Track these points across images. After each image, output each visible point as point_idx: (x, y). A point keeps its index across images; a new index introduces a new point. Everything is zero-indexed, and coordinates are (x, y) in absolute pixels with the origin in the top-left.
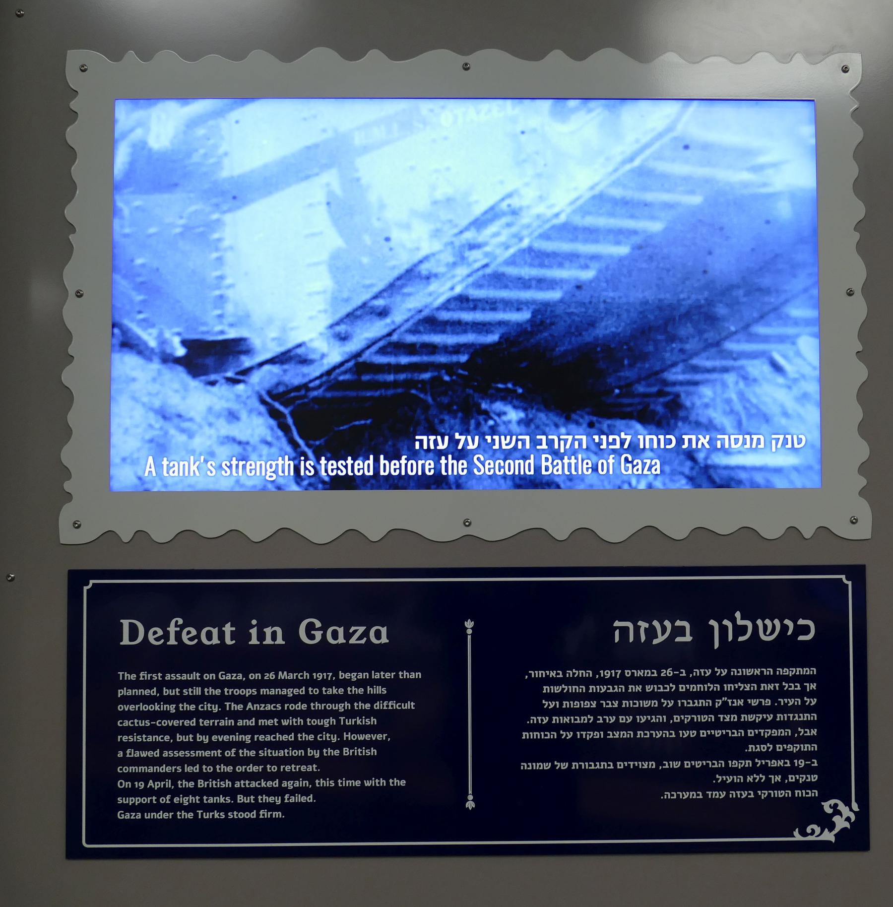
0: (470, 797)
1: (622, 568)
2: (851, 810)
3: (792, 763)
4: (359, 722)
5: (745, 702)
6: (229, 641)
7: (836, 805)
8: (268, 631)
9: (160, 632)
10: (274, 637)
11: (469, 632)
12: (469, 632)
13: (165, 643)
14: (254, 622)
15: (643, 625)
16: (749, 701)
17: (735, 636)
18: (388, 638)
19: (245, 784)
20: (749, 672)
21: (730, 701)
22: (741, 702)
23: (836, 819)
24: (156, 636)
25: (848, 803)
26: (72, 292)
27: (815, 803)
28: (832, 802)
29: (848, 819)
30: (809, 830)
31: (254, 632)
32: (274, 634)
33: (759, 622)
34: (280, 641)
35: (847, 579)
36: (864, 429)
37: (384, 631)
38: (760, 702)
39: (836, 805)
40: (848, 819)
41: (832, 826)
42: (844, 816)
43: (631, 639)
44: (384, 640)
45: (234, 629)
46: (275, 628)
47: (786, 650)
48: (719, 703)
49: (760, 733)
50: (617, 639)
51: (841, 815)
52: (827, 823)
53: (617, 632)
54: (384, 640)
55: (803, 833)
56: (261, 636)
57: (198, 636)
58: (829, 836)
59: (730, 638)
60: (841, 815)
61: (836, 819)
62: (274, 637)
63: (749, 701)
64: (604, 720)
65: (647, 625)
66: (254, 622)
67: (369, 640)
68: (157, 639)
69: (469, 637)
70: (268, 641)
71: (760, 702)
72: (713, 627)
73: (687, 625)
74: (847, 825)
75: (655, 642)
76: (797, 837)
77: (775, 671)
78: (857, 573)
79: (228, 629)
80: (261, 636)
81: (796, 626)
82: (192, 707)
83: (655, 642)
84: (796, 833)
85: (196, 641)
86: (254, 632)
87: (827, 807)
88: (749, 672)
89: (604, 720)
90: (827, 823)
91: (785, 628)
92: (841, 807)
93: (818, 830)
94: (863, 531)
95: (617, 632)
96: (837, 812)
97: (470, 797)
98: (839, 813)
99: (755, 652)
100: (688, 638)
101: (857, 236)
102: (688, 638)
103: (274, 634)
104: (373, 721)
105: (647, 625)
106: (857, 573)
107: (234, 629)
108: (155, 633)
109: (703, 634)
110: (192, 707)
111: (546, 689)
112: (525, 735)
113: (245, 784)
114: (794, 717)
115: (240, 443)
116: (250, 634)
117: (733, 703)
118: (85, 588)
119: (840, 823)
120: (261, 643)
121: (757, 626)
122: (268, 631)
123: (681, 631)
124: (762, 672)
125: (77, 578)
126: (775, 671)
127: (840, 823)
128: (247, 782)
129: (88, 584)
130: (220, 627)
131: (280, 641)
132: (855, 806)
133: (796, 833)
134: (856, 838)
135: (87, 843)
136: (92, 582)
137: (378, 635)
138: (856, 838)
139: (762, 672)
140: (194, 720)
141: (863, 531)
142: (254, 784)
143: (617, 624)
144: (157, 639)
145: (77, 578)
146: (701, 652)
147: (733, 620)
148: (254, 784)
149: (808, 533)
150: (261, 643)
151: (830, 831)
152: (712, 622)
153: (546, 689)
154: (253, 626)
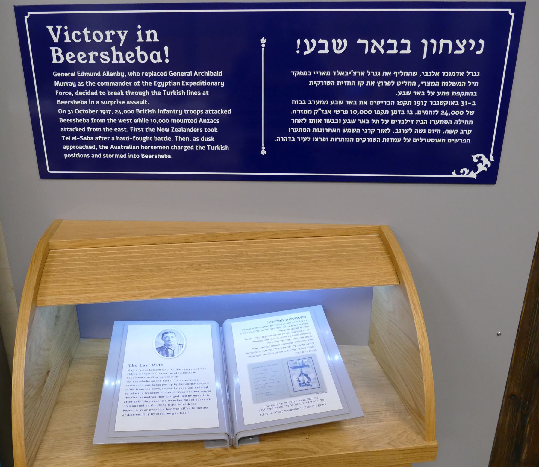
0: (263, 148)
2: (489, 160)
4: (174, 94)
5: (332, 112)
7: (480, 157)
8: (148, 33)
9: (73, 55)
10: (152, 37)
13: (88, 62)
14: (139, 27)
16: (335, 111)
17: (453, 50)
19: (211, 112)
21: (323, 111)
22: (329, 112)
24: (131, 57)
25: (488, 156)
28: (478, 155)
29: (486, 166)
30: (462, 171)
31: (139, 33)
32: (152, 35)
33: (334, 41)
35: (512, 12)
38: (342, 112)
39: (480, 157)
40: (486, 166)
41: (476, 169)
42: (484, 163)
43: (366, 52)
47: (468, 60)
48: (316, 112)
49: (398, 122)
51: (483, 163)
52: (473, 167)
55: (458, 173)
56: (144, 36)
57: (76, 58)
58: (473, 175)
59: (450, 51)
60: (483, 163)
62: (152, 37)
63: (335, 111)
64: (313, 103)
69: (263, 49)
70: (149, 40)
71: (342, 112)
72: (423, 44)
73: (408, 42)
74: (485, 169)
75: (306, 53)
76: (454, 175)
80: (144, 36)
81: (317, 44)
83: (306, 53)
84: (454, 173)
85: (134, 60)
86: (139, 33)
87: (475, 158)
89: (313, 103)
90: (473, 167)
92: (484, 158)
93: (467, 171)
97: (263, 148)
98: (482, 162)
100: (408, 51)
102: (408, 51)
103: (152, 35)
108: (130, 55)
113: (211, 112)
117: (325, 112)
119: (481, 168)
120: (145, 41)
121: (332, 44)
122: (148, 33)
123: (404, 47)
125: (20, 11)
128: (212, 111)
129: (27, 15)
130: (81, 30)
131: (156, 39)
132: (492, 158)
133: (454, 173)
135: (50, 170)
136: (29, 13)
137: (155, 57)
138: (489, 177)
150: (145, 41)
151: (474, 172)
152: (424, 41)
154: (139, 30)
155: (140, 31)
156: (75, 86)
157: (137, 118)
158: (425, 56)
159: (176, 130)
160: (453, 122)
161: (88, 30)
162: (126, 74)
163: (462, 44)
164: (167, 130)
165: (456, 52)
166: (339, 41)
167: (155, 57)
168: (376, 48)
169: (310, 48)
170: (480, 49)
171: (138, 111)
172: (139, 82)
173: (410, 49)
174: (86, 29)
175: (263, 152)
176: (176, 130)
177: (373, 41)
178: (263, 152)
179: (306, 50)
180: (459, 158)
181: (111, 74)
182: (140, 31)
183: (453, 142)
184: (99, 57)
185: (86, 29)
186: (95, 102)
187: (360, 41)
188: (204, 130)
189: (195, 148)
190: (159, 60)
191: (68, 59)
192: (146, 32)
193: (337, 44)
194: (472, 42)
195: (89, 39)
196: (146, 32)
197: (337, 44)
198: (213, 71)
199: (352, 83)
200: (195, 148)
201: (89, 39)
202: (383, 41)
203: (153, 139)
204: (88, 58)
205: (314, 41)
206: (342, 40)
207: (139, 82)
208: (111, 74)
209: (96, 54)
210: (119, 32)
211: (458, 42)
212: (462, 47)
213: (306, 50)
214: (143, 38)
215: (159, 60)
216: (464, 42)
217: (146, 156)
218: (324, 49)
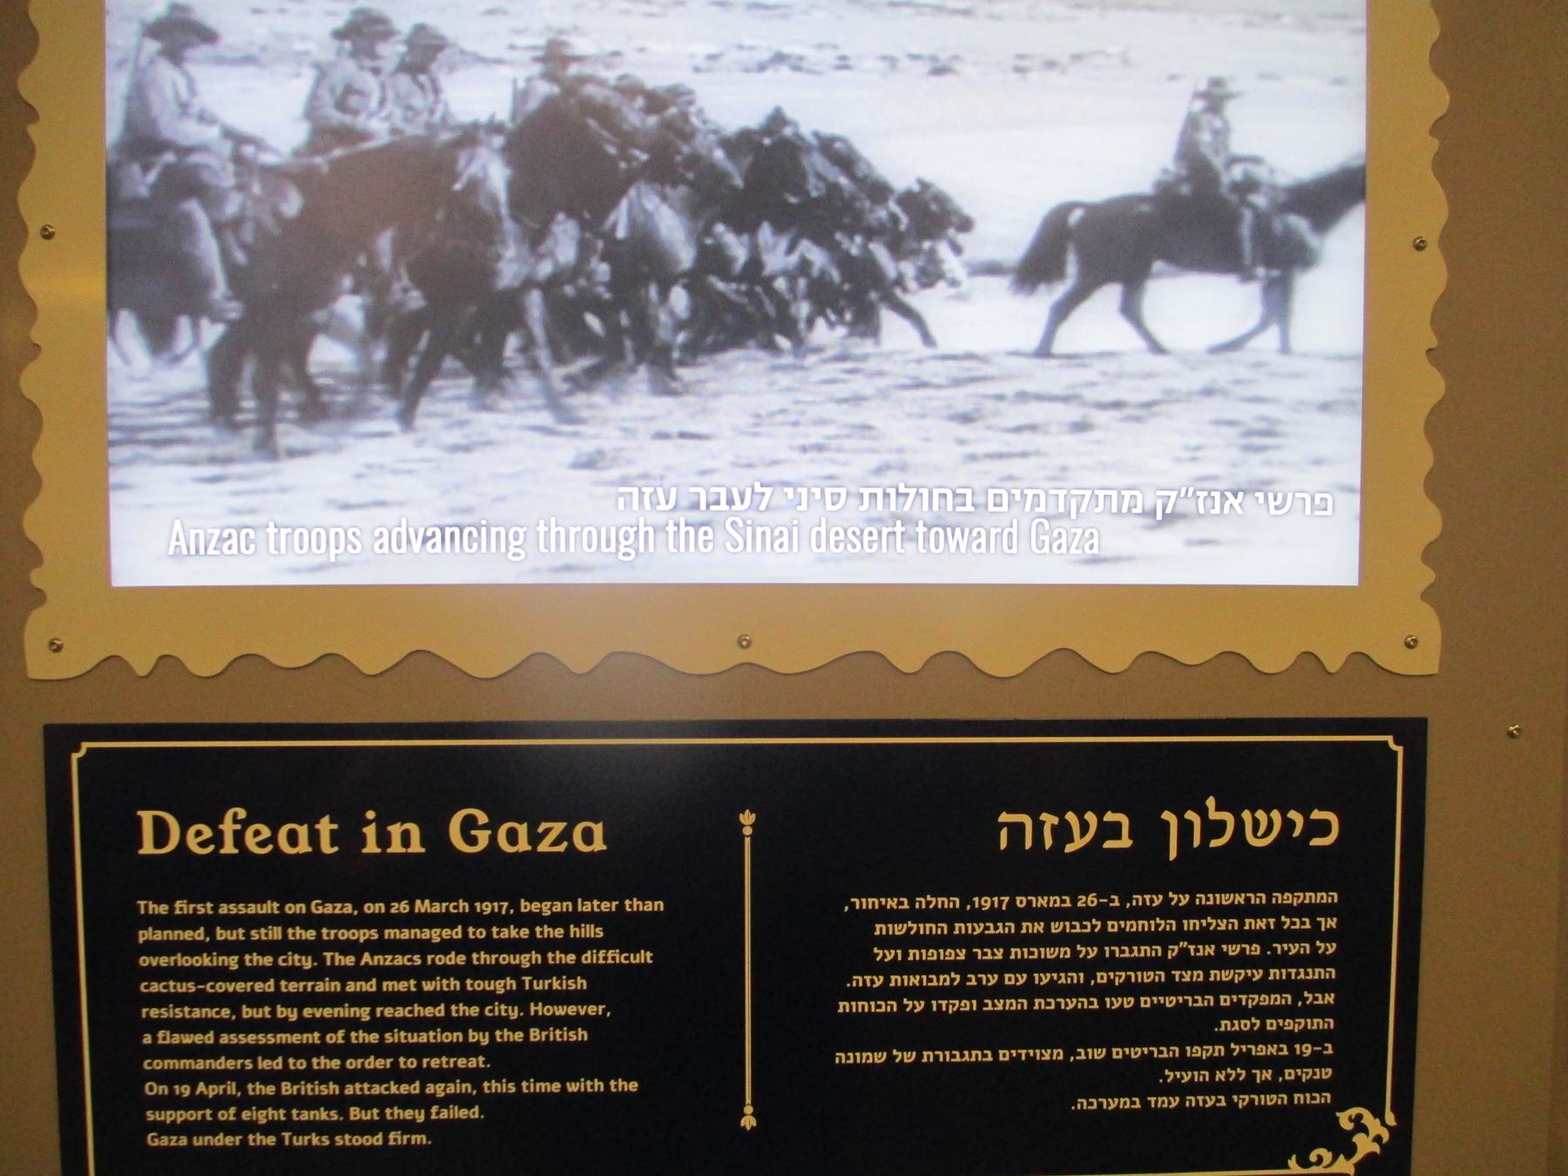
0: (749, 1109)
1: (1110, 721)
2: (1383, 1124)
3: (1291, 1050)
6: (327, 848)
7: (1359, 1117)
8: (395, 830)
9: (207, 833)
11: (748, 831)
12: (748, 831)
15: (1049, 820)
17: (1206, 838)
18: (423, 845)
20: (1225, 899)
23: (1358, 1139)
24: (200, 839)
25: (1379, 1113)
26: (34, 228)
27: (1326, 1116)
28: (1354, 1111)
30: (1313, 1157)
31: (370, 831)
32: (406, 836)
34: (416, 847)
35: (1397, 742)
37: (598, 829)
39: (1359, 1117)
40: (1378, 1139)
41: (1350, 1151)
43: (1028, 844)
44: (599, 845)
45: (335, 826)
47: (1289, 863)
50: (1003, 844)
53: (1004, 833)
54: (599, 845)
55: (1304, 1163)
56: (384, 839)
57: (273, 840)
59: (1197, 843)
61: (1358, 1139)
65: (1055, 820)
67: (571, 846)
69: (747, 841)
70: (396, 847)
72: (1167, 824)
73: (1124, 819)
74: (1376, 1148)
75: (1069, 848)
77: (1269, 898)
78: (1413, 732)
79: (325, 826)
80: (384, 839)
81: (1102, 825)
83: (1069, 848)
84: (1292, 1162)
85: (270, 847)
86: (370, 831)
87: (1345, 1120)
88: (1225, 899)
91: (1288, 825)
92: (1368, 1119)
93: (1327, 1155)
94: (1426, 661)
95: (1004, 833)
96: (1360, 1128)
97: (749, 1109)
98: (1365, 1130)
100: (1125, 842)
101: (1434, 144)
102: (1125, 842)
103: (406, 836)
104: (581, 983)
105: (1055, 820)
106: (1413, 732)
107: (335, 826)
108: (198, 833)
109: (1149, 833)
111: (880, 929)
114: (1298, 974)
118: (75, 757)
119: (1365, 1145)
122: (395, 830)
123: (1113, 831)
124: (1248, 900)
125: (60, 739)
126: (1269, 898)
129: (77, 749)
131: (416, 847)
132: (1390, 1119)
133: (1292, 1162)
137: (588, 837)
139: (1248, 900)
141: (1426, 661)
143: (1004, 817)
145: (60, 739)
146: (1144, 867)
147: (1203, 812)
151: (1348, 1157)
152: (1167, 816)
153: (880, 929)
154: (369, 822)
155: (373, 826)
156: (294, 1017)
157: (432, 978)
158: (1173, 855)
161: (332, 822)
162: (358, 906)
166: (1260, 814)
169: (1083, 834)
171: (232, 962)
173: (1130, 837)
174: (326, 819)
175: (749, 1122)
178: (749, 1122)
179: (1071, 840)
181: (437, 908)
182: (373, 826)
183: (1126, 1057)
185: (326, 819)
191: (193, 843)
192: (390, 828)
195: (332, 845)
196: (390, 828)
198: (642, 899)
199: (319, 908)
200: (448, 1010)
201: (332, 845)
203: (273, 1012)
205: (1091, 817)
206: (1268, 812)
208: (437, 908)
213: (1071, 840)
214: (379, 845)
217: (164, 1141)
218: (1119, 837)
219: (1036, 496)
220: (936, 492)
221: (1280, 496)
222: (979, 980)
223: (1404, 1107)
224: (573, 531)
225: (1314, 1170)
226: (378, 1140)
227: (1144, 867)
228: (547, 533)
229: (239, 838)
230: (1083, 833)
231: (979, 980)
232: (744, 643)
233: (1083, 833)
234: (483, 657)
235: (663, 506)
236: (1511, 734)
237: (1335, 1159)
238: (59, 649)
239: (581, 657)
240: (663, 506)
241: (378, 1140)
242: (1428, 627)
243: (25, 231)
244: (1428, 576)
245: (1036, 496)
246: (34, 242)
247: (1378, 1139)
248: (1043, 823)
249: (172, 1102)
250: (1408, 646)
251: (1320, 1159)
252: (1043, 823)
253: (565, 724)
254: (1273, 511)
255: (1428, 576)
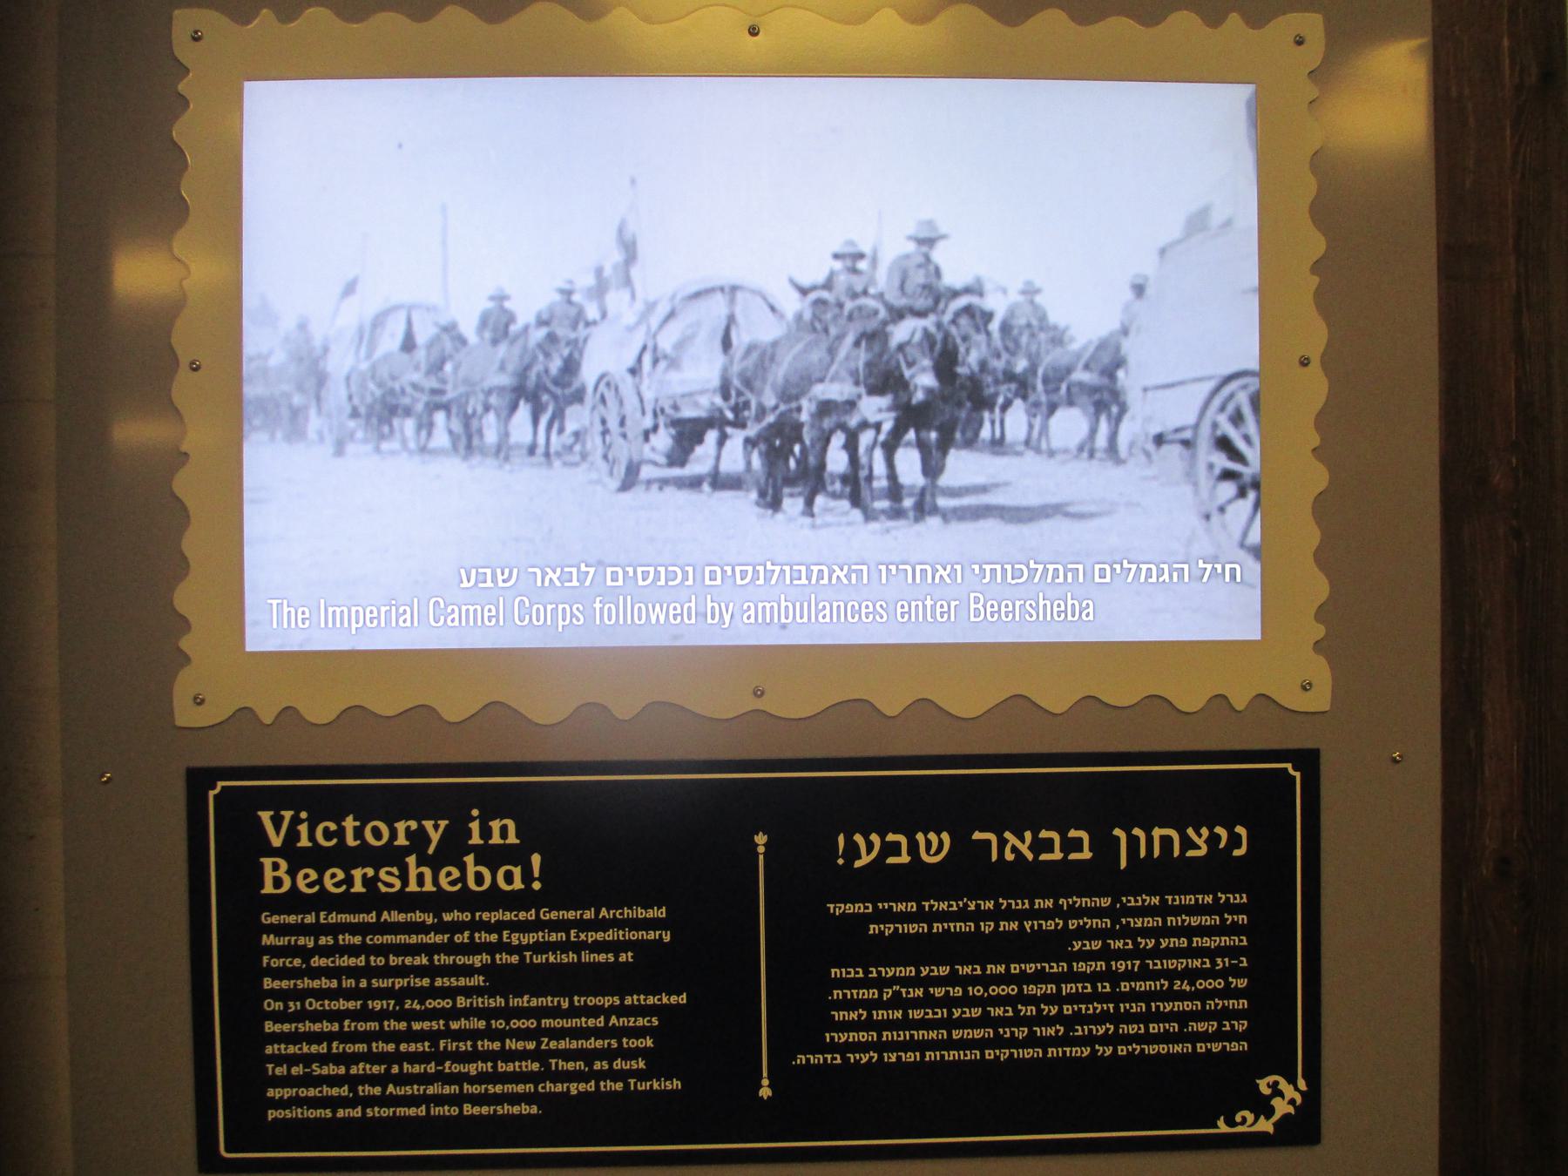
0: (765, 1082)
1: (987, 756)
2: (1296, 1089)
5: (926, 992)
8: (496, 825)
13: (347, 890)
14: (475, 812)
17: (1183, 850)
22: (920, 992)
23: (1276, 1102)
25: (1292, 1080)
26: (184, 361)
28: (1271, 1079)
30: (1238, 1119)
31: (475, 826)
32: (504, 829)
33: (920, 837)
35: (1295, 769)
36: (1322, 558)
39: (1276, 1083)
40: (1292, 1102)
41: (1269, 1112)
42: (1287, 1098)
43: (994, 857)
46: (506, 821)
47: (1217, 871)
48: (888, 994)
55: (1231, 1122)
56: (486, 833)
58: (1265, 1126)
59: (1176, 853)
61: (1276, 1102)
66: (475, 812)
68: (337, 885)
70: (496, 839)
72: (1118, 839)
74: (1291, 1110)
75: (858, 864)
76: (1222, 1127)
78: (1308, 760)
80: (486, 833)
82: (357, 940)
83: (858, 864)
84: (1221, 1123)
86: (475, 826)
87: (1264, 1086)
92: (1283, 1085)
93: (1250, 1117)
94: (1319, 700)
96: (1278, 1093)
97: (765, 1082)
98: (1281, 1094)
99: (1164, 874)
100: (1086, 854)
101: (1315, 280)
102: (1086, 854)
103: (504, 829)
106: (1308, 760)
109: (1105, 846)
110: (357, 940)
112: (272, 1114)
115: (428, 309)
116: (470, 830)
118: (212, 793)
119: (1281, 1107)
122: (496, 825)
123: (1077, 845)
125: (199, 779)
127: (1281, 1107)
129: (214, 788)
130: (339, 820)
131: (512, 839)
132: (1302, 1084)
133: (1221, 1123)
134: (1302, 1129)
135: (227, 1150)
137: (509, 878)
140: (363, 958)
141: (1319, 700)
142: (292, 1049)
144: (337, 885)
145: (199, 779)
148: (292, 1049)
149: (1240, 703)
151: (1268, 1117)
152: (1117, 832)
154: (473, 819)
158: (1123, 864)
159: (553, 1045)
160: (1204, 1005)
163: (1200, 836)
164: (531, 1046)
165: (1190, 853)
166: (932, 836)
167: (509, 878)
168: (1014, 849)
169: (868, 853)
170: (1239, 846)
172: (466, 934)
174: (350, 819)
175: (765, 1092)
176: (553, 1045)
177: (1007, 835)
178: (765, 1092)
180: (1230, 1086)
183: (1209, 1051)
184: (376, 878)
186: (357, 983)
187: (977, 835)
188: (620, 1043)
189: (597, 1086)
190: (518, 885)
193: (929, 844)
194: (1221, 831)
197: (929, 844)
200: (597, 1086)
202: (1028, 835)
204: (349, 881)
205: (875, 838)
206: (938, 835)
207: (466, 934)
208: (401, 917)
209: (370, 872)
210: (428, 824)
211: (1190, 831)
212: (1200, 842)
214: (482, 837)
215: (518, 885)
216: (1205, 831)
217: (476, 1110)
218: (899, 854)
219: (821, 571)
220: (918, 568)
221: (507, 571)
222: (879, 973)
223: (1313, 1074)
224: (549, 607)
225: (1240, 1129)
226: (422, 1111)
227: (1096, 874)
228: (601, 610)
229: (358, 833)
230: (869, 851)
231: (879, 973)
232: (759, 693)
233: (869, 851)
234: (547, 708)
235: (465, 584)
236: (1395, 761)
237: (1256, 1120)
238: (202, 702)
239: (625, 707)
240: (465, 584)
241: (422, 1111)
242: (1321, 672)
243: (1324, 364)
244: (1320, 631)
245: (821, 571)
246: (183, 373)
247: (1292, 1102)
248: (1007, 841)
249: (287, 1081)
250: (1304, 688)
251: (1244, 1120)
252: (1007, 841)
253: (558, 763)
254: (501, 584)
255: (1320, 631)
